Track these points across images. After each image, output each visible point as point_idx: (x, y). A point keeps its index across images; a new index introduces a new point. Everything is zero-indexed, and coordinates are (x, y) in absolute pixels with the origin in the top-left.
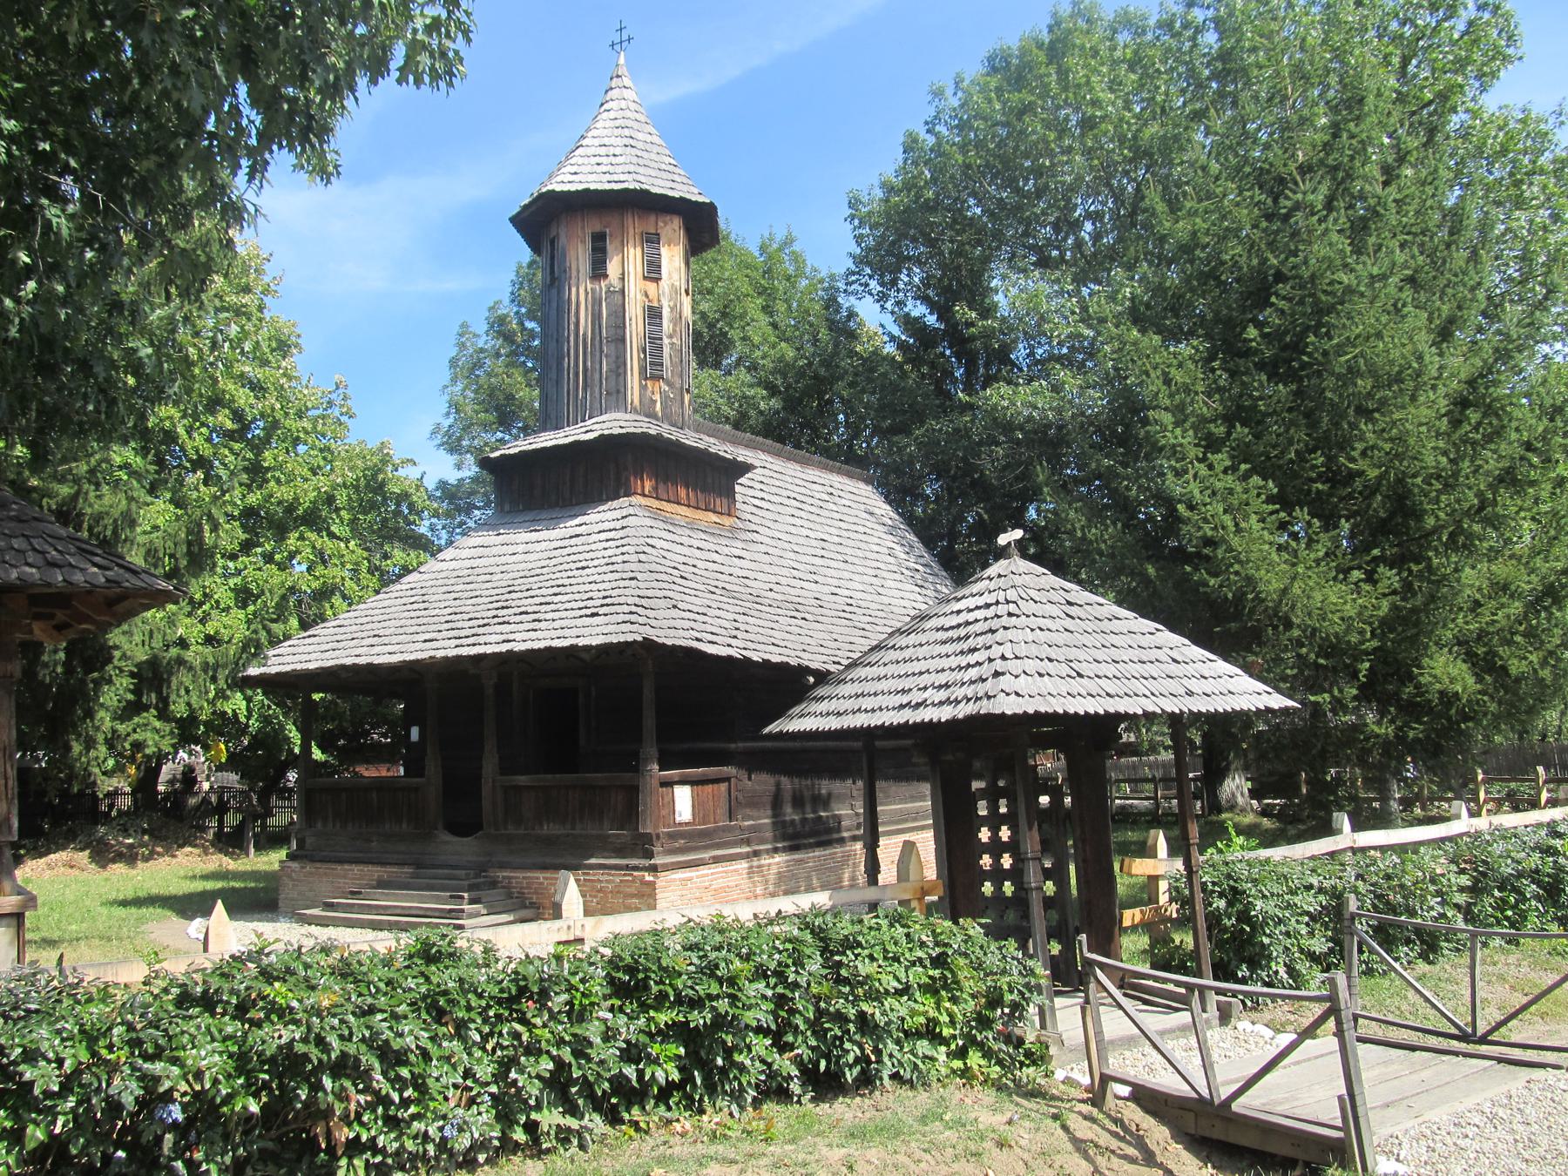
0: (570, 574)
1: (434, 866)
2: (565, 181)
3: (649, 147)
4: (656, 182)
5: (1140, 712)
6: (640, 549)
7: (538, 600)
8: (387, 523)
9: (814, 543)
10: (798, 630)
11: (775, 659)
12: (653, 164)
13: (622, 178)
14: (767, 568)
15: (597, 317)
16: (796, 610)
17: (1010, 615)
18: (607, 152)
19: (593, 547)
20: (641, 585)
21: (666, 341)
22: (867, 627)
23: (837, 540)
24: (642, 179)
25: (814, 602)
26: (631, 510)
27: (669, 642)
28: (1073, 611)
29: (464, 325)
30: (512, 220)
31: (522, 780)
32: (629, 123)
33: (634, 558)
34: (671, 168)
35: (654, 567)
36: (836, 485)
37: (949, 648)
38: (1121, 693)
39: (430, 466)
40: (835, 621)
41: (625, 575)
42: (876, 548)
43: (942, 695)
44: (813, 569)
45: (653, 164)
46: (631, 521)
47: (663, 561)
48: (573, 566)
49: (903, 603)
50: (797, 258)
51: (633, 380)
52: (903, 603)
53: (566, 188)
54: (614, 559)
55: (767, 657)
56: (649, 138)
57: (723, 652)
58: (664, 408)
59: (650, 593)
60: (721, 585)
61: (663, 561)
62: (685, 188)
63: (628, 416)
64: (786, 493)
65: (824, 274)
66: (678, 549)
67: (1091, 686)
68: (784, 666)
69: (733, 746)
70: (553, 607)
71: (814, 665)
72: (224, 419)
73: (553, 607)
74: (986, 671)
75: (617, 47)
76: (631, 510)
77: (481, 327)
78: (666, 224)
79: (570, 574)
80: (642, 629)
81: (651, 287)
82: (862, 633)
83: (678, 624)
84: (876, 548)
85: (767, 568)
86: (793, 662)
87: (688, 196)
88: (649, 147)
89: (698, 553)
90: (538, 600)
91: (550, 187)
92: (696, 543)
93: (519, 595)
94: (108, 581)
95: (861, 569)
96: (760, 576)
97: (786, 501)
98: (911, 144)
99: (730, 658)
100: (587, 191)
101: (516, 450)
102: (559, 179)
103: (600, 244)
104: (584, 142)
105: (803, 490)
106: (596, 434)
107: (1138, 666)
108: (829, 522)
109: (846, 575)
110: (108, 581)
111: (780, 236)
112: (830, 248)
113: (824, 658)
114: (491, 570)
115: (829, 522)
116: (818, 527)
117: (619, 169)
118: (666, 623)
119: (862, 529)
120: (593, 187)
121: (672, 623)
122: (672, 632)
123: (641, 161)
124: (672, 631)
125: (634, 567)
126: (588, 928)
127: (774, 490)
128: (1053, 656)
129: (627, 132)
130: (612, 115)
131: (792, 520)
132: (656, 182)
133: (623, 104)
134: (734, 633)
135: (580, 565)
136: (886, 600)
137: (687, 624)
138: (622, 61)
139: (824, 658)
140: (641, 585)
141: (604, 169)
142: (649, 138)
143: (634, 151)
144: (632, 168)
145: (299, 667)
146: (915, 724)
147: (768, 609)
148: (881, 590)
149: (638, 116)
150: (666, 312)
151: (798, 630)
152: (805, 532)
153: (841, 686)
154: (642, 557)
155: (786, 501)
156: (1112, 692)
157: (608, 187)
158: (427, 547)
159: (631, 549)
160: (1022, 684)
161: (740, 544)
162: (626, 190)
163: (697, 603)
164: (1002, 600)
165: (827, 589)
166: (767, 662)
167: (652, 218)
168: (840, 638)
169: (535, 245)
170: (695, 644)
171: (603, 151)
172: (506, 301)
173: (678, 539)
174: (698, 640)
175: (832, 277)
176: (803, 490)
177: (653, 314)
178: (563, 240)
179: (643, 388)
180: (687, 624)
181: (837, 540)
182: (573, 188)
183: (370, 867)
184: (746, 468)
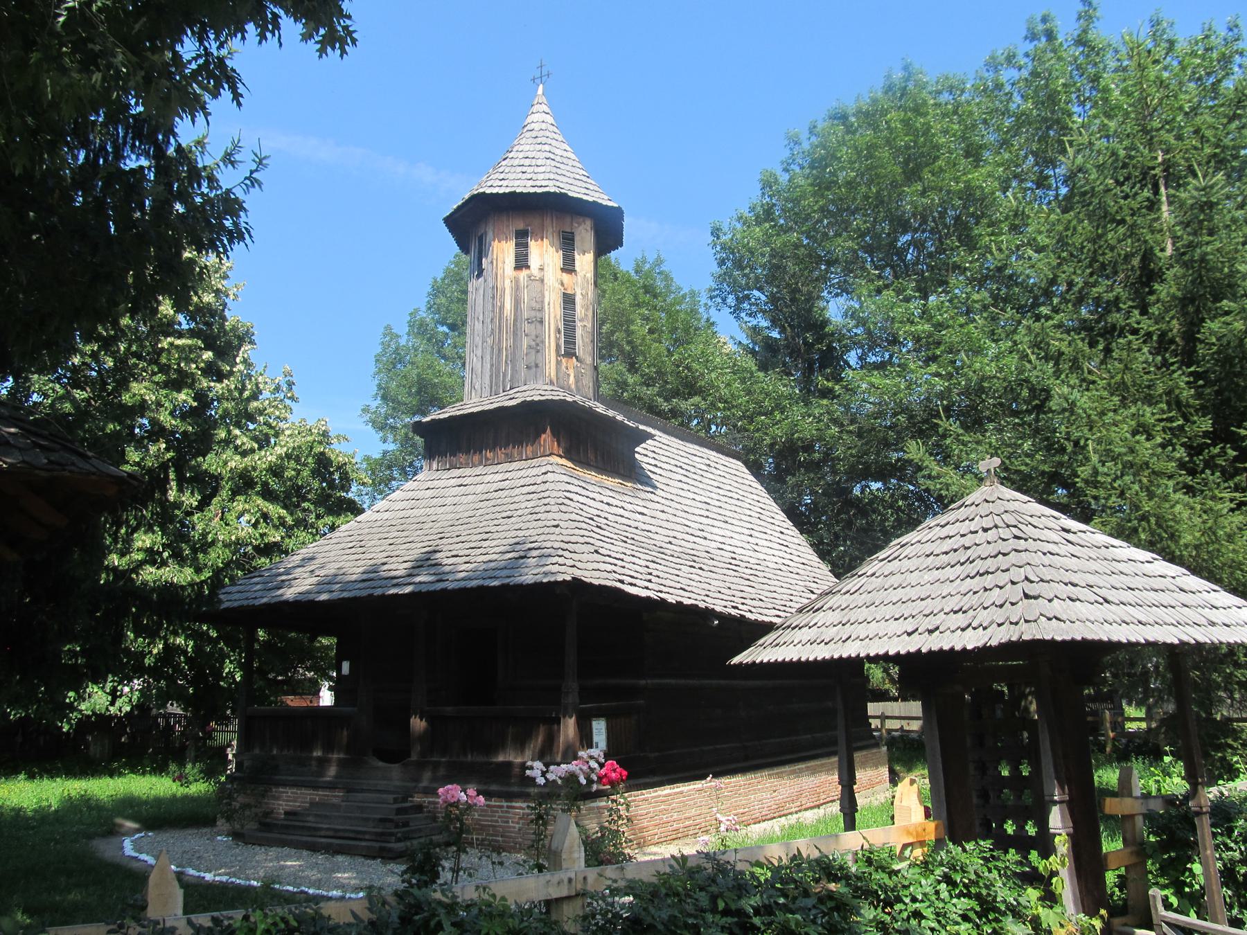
0: (496, 522)
1: (362, 791)
2: (496, 185)
3: (565, 161)
4: (572, 188)
5: (1176, 642)
6: (560, 501)
7: (467, 545)
8: (321, 491)
9: (700, 505)
10: (698, 578)
11: (686, 602)
12: (568, 174)
13: (544, 183)
14: (665, 524)
15: (517, 302)
16: (693, 561)
17: (1016, 537)
18: (537, 161)
19: (516, 499)
20: (564, 532)
21: (578, 324)
22: (751, 578)
23: (718, 504)
24: (562, 185)
25: (706, 555)
26: (549, 468)
27: (596, 582)
28: (1070, 537)
29: (388, 328)
30: (449, 221)
31: (449, 710)
32: (549, 141)
33: (555, 508)
34: (585, 179)
35: (573, 517)
36: (712, 458)
37: (949, 573)
38: (1152, 622)
39: (359, 442)
40: (725, 571)
41: (549, 524)
42: (748, 512)
43: (961, 620)
44: (701, 527)
45: (568, 174)
46: (550, 477)
47: (580, 512)
48: (499, 516)
49: (775, 559)
50: (667, 278)
51: (550, 356)
52: (775, 559)
53: (495, 191)
54: (537, 510)
55: (679, 599)
56: (565, 154)
57: (643, 593)
58: (577, 382)
59: (573, 539)
60: (630, 536)
61: (580, 512)
62: (597, 195)
63: (546, 387)
64: (673, 462)
65: (686, 290)
66: (591, 503)
67: (1122, 612)
68: (693, 609)
69: (643, 682)
70: (482, 551)
71: (718, 609)
72: (184, 397)
73: (482, 551)
74: (1015, 593)
75: (538, 81)
76: (549, 468)
77: (402, 329)
78: (579, 224)
79: (496, 522)
80: (570, 570)
81: (566, 277)
82: (747, 583)
83: (602, 566)
84: (748, 512)
85: (665, 524)
86: (702, 605)
87: (600, 201)
88: (565, 161)
89: (606, 508)
90: (467, 545)
91: (481, 190)
92: (606, 500)
93: (450, 541)
94: (50, 462)
95: (738, 529)
96: (659, 530)
97: (674, 469)
98: (768, 184)
99: (649, 598)
100: (513, 194)
101: (446, 415)
102: (489, 184)
103: (523, 241)
104: (510, 155)
105: (686, 461)
106: (519, 401)
107: (1152, 594)
108: (709, 488)
109: (729, 534)
110: (50, 462)
111: (651, 258)
112: (693, 271)
113: (724, 603)
114: (422, 519)
115: (709, 488)
116: (701, 492)
117: (541, 176)
118: (590, 566)
119: (736, 496)
120: (518, 190)
121: (596, 566)
122: (597, 574)
123: (559, 171)
124: (596, 574)
125: (556, 516)
126: (590, 880)
127: (664, 459)
128: (1076, 581)
129: (547, 148)
130: (534, 134)
131: (680, 485)
132: (572, 188)
133: (544, 126)
134: (649, 577)
135: (505, 515)
136: (762, 556)
137: (610, 568)
138: (540, 91)
139: (724, 603)
140: (564, 532)
141: (529, 176)
142: (565, 154)
143: (553, 163)
144: (552, 176)
145: (245, 603)
146: (930, 652)
147: (671, 559)
148: (756, 548)
149: (556, 136)
150: (578, 299)
151: (698, 578)
152: (691, 496)
153: (821, 614)
154: (563, 508)
155: (674, 469)
156: (1144, 620)
157: (532, 190)
158: (355, 509)
159: (552, 501)
160: (1057, 607)
161: (641, 503)
162: (548, 193)
163: (619, 548)
164: (1000, 524)
165: (714, 545)
166: (679, 604)
167: (568, 219)
168: (733, 586)
169: (464, 248)
170: (619, 585)
171: (527, 162)
172: (424, 309)
173: (591, 495)
174: (622, 582)
175: (693, 294)
176: (686, 461)
177: (569, 300)
178: (490, 235)
179: (558, 363)
180: (610, 568)
181: (718, 504)
182: (501, 191)
183: (304, 791)
184: (651, 436)
